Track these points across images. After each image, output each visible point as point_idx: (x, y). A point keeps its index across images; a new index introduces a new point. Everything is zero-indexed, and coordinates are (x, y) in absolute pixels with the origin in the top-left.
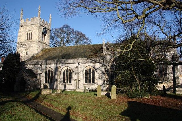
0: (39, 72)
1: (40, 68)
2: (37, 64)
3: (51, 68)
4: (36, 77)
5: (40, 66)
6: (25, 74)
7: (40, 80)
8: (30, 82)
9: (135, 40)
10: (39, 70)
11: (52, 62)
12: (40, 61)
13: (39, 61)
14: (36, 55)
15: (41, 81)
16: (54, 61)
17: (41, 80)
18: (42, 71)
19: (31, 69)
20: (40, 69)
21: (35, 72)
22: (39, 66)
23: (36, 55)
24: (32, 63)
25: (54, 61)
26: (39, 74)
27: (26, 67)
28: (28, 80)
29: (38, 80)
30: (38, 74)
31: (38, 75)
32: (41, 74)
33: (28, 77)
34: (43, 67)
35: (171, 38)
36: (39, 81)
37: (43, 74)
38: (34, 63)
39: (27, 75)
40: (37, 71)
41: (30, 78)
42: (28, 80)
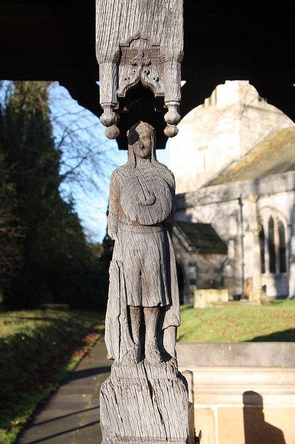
0: (234, 230)
1: (238, 217)
2: (226, 198)
3: (278, 211)
4: (223, 249)
5: (238, 207)
6: (179, 240)
7: (240, 262)
8: (198, 270)
9: (47, 219)
10: (232, 222)
11: (276, 182)
12: (236, 187)
13: (231, 184)
14: (234, 165)
15: (243, 265)
16: (284, 178)
17: (245, 261)
18: (245, 225)
19: (206, 220)
20: (237, 220)
21: (221, 232)
22: (234, 205)
23: (234, 165)
24: (209, 196)
25: (284, 178)
26: (235, 239)
27: (190, 217)
28: (191, 265)
29: (233, 263)
30: (231, 239)
31: (232, 243)
32: (243, 236)
33: (187, 251)
34: (249, 208)
35: (22, 106)
36: (234, 269)
37: (251, 240)
38: (216, 198)
39: (186, 245)
40: (227, 229)
41: (196, 258)
42: (191, 265)
